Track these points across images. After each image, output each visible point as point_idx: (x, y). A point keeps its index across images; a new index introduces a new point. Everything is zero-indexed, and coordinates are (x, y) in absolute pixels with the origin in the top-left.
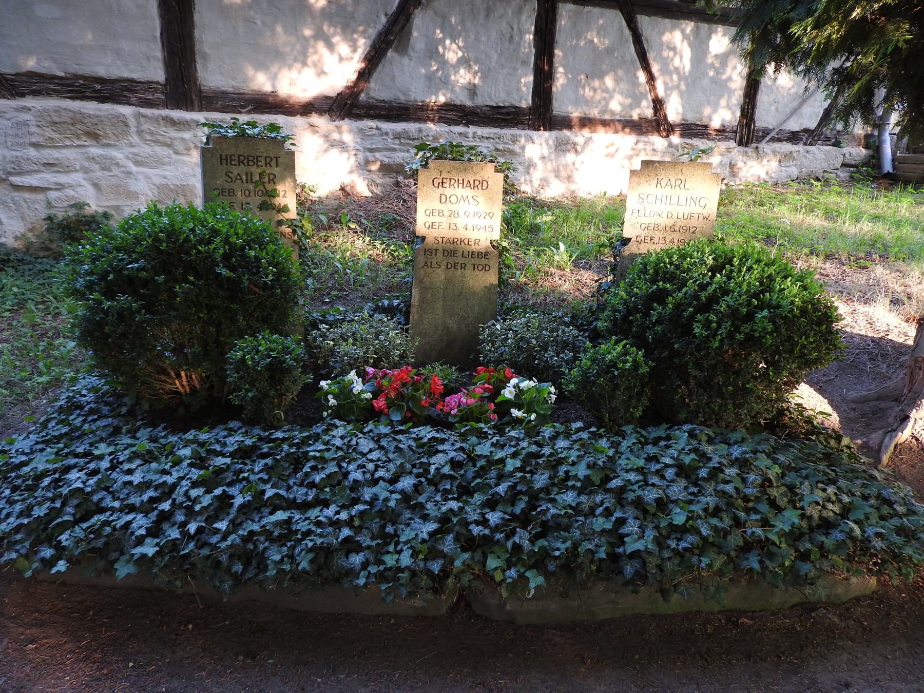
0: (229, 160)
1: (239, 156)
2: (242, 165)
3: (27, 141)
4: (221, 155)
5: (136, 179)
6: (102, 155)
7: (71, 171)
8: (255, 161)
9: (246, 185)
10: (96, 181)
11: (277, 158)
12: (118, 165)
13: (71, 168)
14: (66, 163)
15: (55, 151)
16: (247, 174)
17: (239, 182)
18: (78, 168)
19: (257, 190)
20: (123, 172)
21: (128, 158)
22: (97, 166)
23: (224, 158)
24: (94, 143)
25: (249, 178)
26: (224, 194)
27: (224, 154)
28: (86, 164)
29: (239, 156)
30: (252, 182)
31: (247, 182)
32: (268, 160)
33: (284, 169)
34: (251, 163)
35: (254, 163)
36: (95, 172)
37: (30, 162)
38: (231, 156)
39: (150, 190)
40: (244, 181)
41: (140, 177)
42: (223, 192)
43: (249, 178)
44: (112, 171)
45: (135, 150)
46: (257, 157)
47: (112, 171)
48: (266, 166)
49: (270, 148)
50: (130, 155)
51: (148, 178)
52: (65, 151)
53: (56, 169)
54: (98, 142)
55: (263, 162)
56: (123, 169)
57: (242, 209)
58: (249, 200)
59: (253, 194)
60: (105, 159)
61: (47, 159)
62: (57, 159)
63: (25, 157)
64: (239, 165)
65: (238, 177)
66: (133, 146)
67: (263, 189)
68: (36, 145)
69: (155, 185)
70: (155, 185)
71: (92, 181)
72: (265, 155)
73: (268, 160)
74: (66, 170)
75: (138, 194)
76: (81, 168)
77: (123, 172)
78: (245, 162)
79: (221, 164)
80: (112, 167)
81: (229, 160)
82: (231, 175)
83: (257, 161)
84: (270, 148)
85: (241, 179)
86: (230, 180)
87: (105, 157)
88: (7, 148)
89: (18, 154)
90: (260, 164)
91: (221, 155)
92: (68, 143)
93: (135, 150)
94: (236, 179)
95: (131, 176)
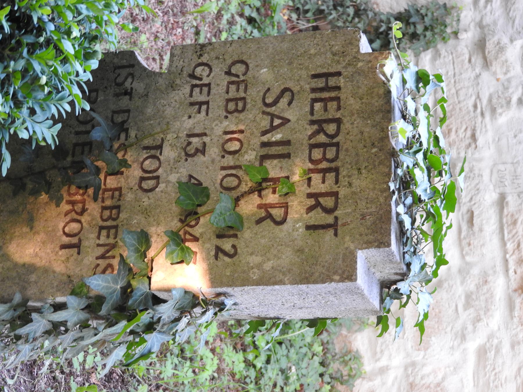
0: (326, 95)
1: (338, 121)
2: (311, 129)
3: (508, 190)
4: (339, 74)
5: (452, 348)
6: (492, 296)
7: (462, 250)
8: (324, 165)
9: (256, 141)
10: (446, 285)
11: (334, 226)
12: (478, 319)
13: (467, 249)
14: (475, 242)
15: (494, 227)
16: (286, 143)
17: (265, 123)
18: (468, 259)
19: (240, 173)
20: (464, 328)
21: (490, 337)
22: (472, 287)
23: (332, 82)
24: (514, 285)
25: (274, 150)
26: (233, 88)
27: (341, 81)
28: (475, 271)
29: (338, 121)
30: (264, 158)
31: (264, 145)
32: (328, 202)
33: (300, 251)
34: (317, 154)
35: (319, 162)
36: (462, 283)
37: (473, 192)
38: (337, 99)
39: (434, 372)
40: (265, 139)
41: (457, 355)
42: (238, 83)
43: (274, 150)
44: (465, 310)
45: (506, 349)
46: (336, 170)
47: (465, 310)
48: (310, 196)
49: (362, 204)
50: (496, 341)
51: (456, 368)
52: (496, 242)
53: (464, 227)
54: (515, 291)
55: (323, 188)
56: (470, 327)
57: (189, 136)
58: (213, 151)
59: (229, 160)
60: (487, 301)
61: (480, 215)
62: (481, 230)
63: (481, 186)
64: (312, 122)
65: (277, 122)
66: (513, 347)
67: (244, 188)
68: (502, 202)
69: (444, 379)
70: (444, 379)
71: (446, 280)
72: (343, 192)
73: (328, 202)
74: (464, 242)
75: (426, 349)
76: (467, 264)
77: (464, 328)
78: (322, 138)
79: (315, 76)
80: (472, 310)
81: (326, 95)
82: (284, 101)
83: (324, 171)
84: (362, 204)
85: (273, 128)
86: (269, 100)
87: (490, 299)
88: (494, 165)
89: (486, 177)
90: (316, 178)
91: (339, 74)
92: (510, 246)
93: (506, 349)
94: (273, 116)
95: (459, 340)
